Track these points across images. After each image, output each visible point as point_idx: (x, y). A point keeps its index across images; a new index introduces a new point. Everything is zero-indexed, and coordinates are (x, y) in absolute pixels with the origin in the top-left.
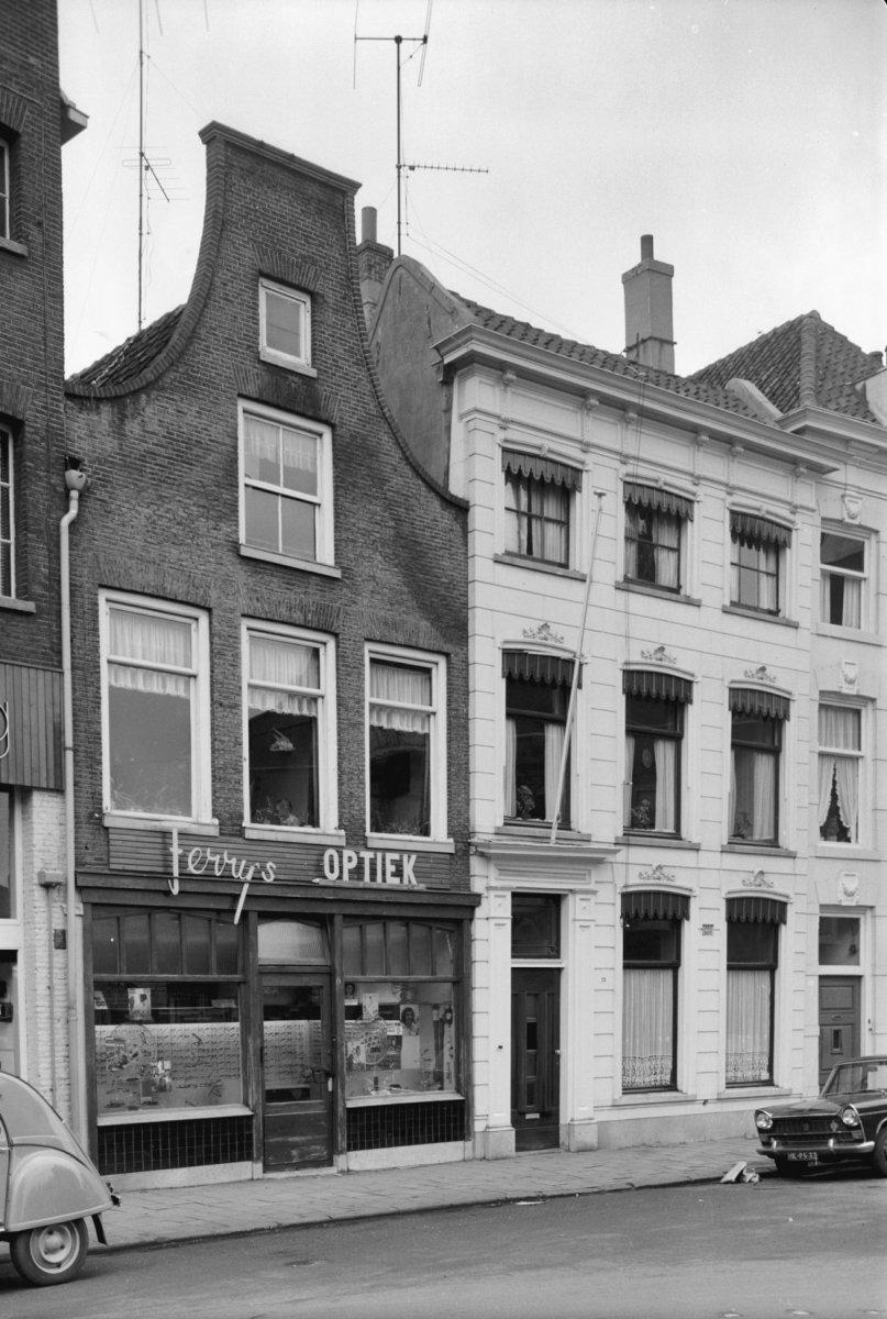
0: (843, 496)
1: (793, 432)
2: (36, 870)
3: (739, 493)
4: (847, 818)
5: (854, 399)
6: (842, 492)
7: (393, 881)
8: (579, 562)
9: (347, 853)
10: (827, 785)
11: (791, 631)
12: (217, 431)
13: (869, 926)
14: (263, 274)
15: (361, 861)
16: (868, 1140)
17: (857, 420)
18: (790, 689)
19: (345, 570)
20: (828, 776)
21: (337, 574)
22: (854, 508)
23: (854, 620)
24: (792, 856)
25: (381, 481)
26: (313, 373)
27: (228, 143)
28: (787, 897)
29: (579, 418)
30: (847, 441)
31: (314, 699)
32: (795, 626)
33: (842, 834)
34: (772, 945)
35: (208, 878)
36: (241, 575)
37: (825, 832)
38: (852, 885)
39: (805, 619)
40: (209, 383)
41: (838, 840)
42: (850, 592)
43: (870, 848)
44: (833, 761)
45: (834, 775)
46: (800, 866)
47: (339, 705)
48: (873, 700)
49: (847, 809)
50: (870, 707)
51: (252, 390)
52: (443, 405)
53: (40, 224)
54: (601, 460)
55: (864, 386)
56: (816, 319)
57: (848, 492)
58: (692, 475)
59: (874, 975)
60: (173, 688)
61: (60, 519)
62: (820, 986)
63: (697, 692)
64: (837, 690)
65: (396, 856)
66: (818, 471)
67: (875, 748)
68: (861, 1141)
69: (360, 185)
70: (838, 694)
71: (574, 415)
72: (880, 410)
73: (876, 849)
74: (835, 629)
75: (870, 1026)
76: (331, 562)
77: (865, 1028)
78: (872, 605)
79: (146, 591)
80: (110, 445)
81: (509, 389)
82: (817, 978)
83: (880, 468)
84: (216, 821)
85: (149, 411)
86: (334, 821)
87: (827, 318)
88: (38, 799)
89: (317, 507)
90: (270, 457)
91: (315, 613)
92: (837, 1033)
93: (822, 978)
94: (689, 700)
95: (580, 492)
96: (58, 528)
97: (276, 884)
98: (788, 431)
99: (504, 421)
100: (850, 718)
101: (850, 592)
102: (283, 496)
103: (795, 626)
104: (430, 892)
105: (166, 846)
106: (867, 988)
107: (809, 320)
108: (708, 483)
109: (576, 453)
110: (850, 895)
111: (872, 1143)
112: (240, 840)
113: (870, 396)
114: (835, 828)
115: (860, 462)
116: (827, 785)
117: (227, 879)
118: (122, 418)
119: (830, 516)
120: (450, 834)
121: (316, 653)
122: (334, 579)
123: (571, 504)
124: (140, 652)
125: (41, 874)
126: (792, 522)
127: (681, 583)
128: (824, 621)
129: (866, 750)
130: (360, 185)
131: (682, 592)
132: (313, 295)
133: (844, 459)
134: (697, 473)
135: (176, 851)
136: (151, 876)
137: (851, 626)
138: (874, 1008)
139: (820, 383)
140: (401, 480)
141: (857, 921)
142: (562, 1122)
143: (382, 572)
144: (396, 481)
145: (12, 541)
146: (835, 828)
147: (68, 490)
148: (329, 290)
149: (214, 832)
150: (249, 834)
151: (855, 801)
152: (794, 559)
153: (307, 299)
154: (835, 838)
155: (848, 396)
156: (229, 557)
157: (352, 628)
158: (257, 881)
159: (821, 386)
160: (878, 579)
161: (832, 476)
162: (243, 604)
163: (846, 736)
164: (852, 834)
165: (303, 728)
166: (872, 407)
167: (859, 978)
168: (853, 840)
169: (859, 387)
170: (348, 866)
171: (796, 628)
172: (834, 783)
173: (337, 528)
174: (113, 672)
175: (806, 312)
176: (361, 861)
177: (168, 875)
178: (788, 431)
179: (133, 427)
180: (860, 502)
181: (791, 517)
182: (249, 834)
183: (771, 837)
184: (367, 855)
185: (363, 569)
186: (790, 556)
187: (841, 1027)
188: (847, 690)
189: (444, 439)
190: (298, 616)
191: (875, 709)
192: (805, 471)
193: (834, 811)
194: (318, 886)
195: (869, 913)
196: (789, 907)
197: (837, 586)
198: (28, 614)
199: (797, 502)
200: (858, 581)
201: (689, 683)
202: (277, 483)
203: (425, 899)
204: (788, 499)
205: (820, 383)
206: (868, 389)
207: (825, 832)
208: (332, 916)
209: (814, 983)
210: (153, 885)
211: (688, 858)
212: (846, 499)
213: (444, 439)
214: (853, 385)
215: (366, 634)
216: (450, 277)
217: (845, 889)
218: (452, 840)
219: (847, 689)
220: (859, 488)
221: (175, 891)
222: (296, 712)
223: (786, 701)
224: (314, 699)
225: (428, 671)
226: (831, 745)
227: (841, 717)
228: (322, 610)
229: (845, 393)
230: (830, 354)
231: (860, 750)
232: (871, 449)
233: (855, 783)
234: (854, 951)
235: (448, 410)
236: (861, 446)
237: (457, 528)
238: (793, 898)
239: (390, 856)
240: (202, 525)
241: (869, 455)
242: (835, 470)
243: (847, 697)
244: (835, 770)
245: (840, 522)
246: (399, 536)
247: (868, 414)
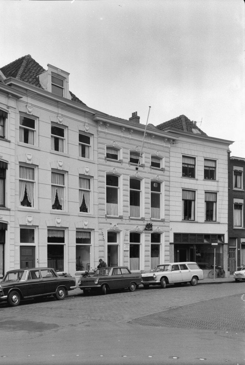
0: (84, 125)
1: (8, 85)
3: (11, 108)
4: (30, 199)
5: (35, 80)
6: (26, 105)
8: (7, 137)
10: (23, 190)
11: (8, 143)
13: (93, 234)
16: (5, 295)
17: (34, 86)
18: (7, 160)
20: (23, 188)
22: (30, 110)
23: (32, 142)
24: (9, 210)
28: (7, 222)
29: (7, 101)
30: (26, 90)
32: (9, 142)
33: (29, 205)
34: (4, 236)
37: (23, 203)
38: (59, 221)
39: (12, 140)
41: (28, 206)
42: (31, 135)
43: (67, 211)
44: (25, 183)
45: (26, 187)
46: (12, 213)
48: (38, 166)
49: (30, 198)
50: (37, 168)
54: (12, 110)
55: (39, 77)
56: (29, 57)
57: (28, 105)
58: (7, 105)
59: (39, 246)
62: (20, 248)
63: (9, 166)
64: (25, 162)
66: (17, 98)
67: (68, 185)
68: (3, 296)
70: (84, 175)
71: (5, 98)
72: (43, 84)
73: (39, 209)
74: (83, 159)
75: (38, 261)
77: (36, 261)
78: (37, 139)
81: (9, 99)
82: (19, 247)
83: (51, 104)
87: (33, 57)
92: (27, 263)
93: (21, 246)
94: (6, 168)
95: (7, 118)
98: (6, 84)
99: (8, 106)
100: (61, 177)
101: (31, 135)
103: (9, 142)
106: (37, 249)
107: (27, 57)
108: (12, 108)
110: (59, 223)
111: (6, 296)
113: (40, 80)
114: (26, 202)
115: (32, 97)
116: (23, 190)
119: (81, 130)
123: (5, 121)
126: (8, 111)
127: (5, 136)
128: (80, 156)
129: (36, 180)
131: (5, 138)
133: (26, 95)
134: (8, 105)
137: (31, 144)
138: (39, 256)
139: (24, 74)
141: (34, 230)
146: (26, 202)
151: (33, 195)
152: (9, 122)
154: (26, 205)
159: (25, 74)
160: (39, 131)
161: (21, 99)
163: (29, 175)
164: (32, 204)
166: (41, 83)
167: (35, 247)
168: (32, 206)
169: (37, 76)
171: (10, 142)
172: (26, 189)
174: (80, 193)
175: (27, 55)
178: (6, 84)
180: (32, 108)
181: (7, 109)
183: (3, 204)
186: (8, 121)
187: (28, 261)
188: (59, 168)
191: (68, 174)
192: (11, 96)
193: (57, 200)
195: (67, 229)
196: (8, 225)
197: (26, 133)
199: (9, 105)
200: (63, 140)
201: (7, 164)
204: (6, 104)
205: (24, 74)
206: (40, 77)
207: (23, 203)
209: (18, 249)
211: (7, 212)
212: (27, 107)
214: (36, 76)
216: (110, 115)
217: (57, 222)
219: (60, 168)
220: (32, 104)
223: (6, 164)
226: (24, 178)
227: (28, 170)
229: (32, 77)
230: (31, 67)
231: (34, 180)
232: (65, 105)
233: (33, 189)
234: (33, 238)
236: (33, 93)
238: (9, 222)
241: (35, 95)
242: (22, 97)
243: (60, 170)
244: (26, 185)
245: (57, 123)
247: (40, 86)
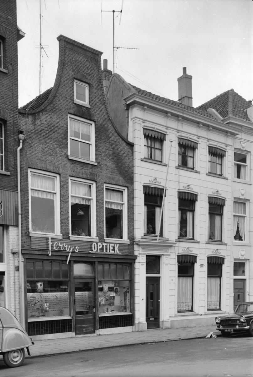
0: (240, 142)
1: (226, 123)
2: (10, 249)
3: (211, 141)
4: (242, 234)
5: (244, 114)
6: (240, 141)
7: (112, 252)
9: (99, 244)
10: (236, 224)
11: (226, 180)
12: (62, 123)
13: (248, 265)
14: (75, 78)
15: (103, 246)
16: (248, 326)
17: (244, 120)
18: (225, 197)
19: (98, 163)
20: (236, 222)
21: (96, 164)
22: (244, 145)
23: (244, 177)
24: (226, 245)
25: (109, 138)
26: (89, 107)
27: (65, 41)
28: (225, 256)
29: (165, 120)
30: (242, 126)
31: (89, 200)
32: (227, 179)
33: (240, 238)
34: (220, 270)
35: (59, 251)
36: (69, 164)
37: (235, 238)
38: (243, 253)
39: (230, 177)
40: (60, 109)
41: (239, 240)
42: (242, 169)
43: (248, 242)
44: (238, 218)
45: (238, 222)
46: (228, 247)
47: (97, 201)
48: (249, 200)
50: (248, 202)
51: (72, 111)
52: (126, 116)
53: (11, 64)
54: (171, 131)
55: (247, 110)
56: (233, 91)
57: (242, 141)
58: (197, 136)
59: (249, 279)
60: (49, 197)
61: (17, 148)
62: (234, 282)
63: (199, 198)
64: (239, 197)
65: (113, 245)
66: (233, 135)
67: (250, 214)
68: (246, 326)
69: (103, 53)
70: (239, 198)
71: (164, 118)
72: (251, 117)
73: (250, 243)
74: (238, 180)
75: (248, 293)
76: (94, 161)
77: (247, 294)
78: (249, 173)
80: (31, 127)
81: (145, 111)
82: (233, 280)
83: (251, 134)
84: (62, 235)
85: (42, 117)
86: (95, 235)
87: (236, 91)
88: (11, 228)
89: (90, 145)
90: (77, 130)
91: (90, 175)
92: (239, 295)
93: (234, 279)
94: (196, 200)
95: (166, 141)
96: (17, 151)
97: (79, 253)
98: (225, 123)
99: (144, 120)
100: (243, 205)
101: (242, 169)
102: (81, 142)
103: (227, 179)
104: (123, 255)
105: (47, 242)
106: (247, 282)
107: (231, 92)
108: (202, 138)
110: (242, 256)
111: (249, 327)
112: (68, 240)
113: (248, 113)
114: (238, 237)
115: (245, 132)
116: (236, 224)
117: (65, 251)
118: (35, 119)
119: (237, 147)
120: (128, 238)
121: (90, 187)
122: (95, 166)
123: (163, 144)
124: (40, 186)
125: (12, 250)
126: (226, 149)
127: (194, 167)
128: (235, 178)
129: (247, 214)
130: (103, 53)
131: (195, 169)
132: (89, 84)
133: (241, 131)
134: (199, 135)
135: (50, 243)
136: (43, 250)
137: (243, 179)
138: (249, 288)
139: (234, 109)
140: (114, 137)
141: (244, 263)
142: (160, 321)
143: (109, 163)
144: (113, 138)
145: (3, 155)
146: (238, 237)
147: (19, 140)
148: (94, 83)
149: (61, 238)
150: (71, 238)
151: (244, 229)
152: (227, 160)
153: (88, 85)
154: (238, 239)
156: (65, 159)
157: (100, 180)
158: (73, 252)
160: (250, 165)
161: (237, 136)
162: (69, 173)
163: (241, 210)
164: (243, 238)
165: (87, 208)
166: (249, 116)
167: (245, 280)
168: (243, 240)
169: (245, 110)
170: (99, 248)
171: (227, 179)
172: (238, 224)
173: (96, 151)
174: (32, 192)
175: (230, 89)
176: (103, 246)
177: (48, 250)
178: (225, 123)
179: (38, 122)
180: (245, 143)
181: (226, 148)
182: (71, 238)
183: (220, 239)
184: (105, 244)
185: (104, 163)
186: (225, 159)
187: (240, 294)
188: (242, 197)
189: (127, 125)
190: (85, 176)
191: (250, 203)
192: (230, 135)
193: (238, 232)
194: (91, 253)
195: (248, 261)
196: (225, 259)
197: (239, 168)
198: (8, 176)
199: (227, 143)
200: (245, 166)
201: (197, 195)
202: (79, 138)
203: (121, 257)
204: (225, 143)
205: (234, 109)
206: (248, 111)
207: (235, 238)
208: (95, 262)
209: (232, 281)
210: (44, 253)
211: (196, 245)
212: (241, 143)
213: (127, 125)
214: (243, 110)
215: (104, 181)
216: (128, 79)
217: (241, 254)
218: (129, 240)
219: (242, 197)
220: (245, 139)
221: (50, 255)
222: (84, 203)
223: (224, 200)
224: (89, 200)
225: (122, 192)
226: (237, 213)
227: (240, 205)
228: (92, 174)
229: (241, 112)
230: (237, 101)
231: (245, 214)
232: (248, 128)
233: (244, 224)
234: (244, 272)
235: (128, 117)
236: (246, 128)
237: (130, 151)
238: (226, 257)
239: (111, 245)
240: (58, 150)
241: (248, 130)
242: (238, 134)
243: (242, 199)
244: (238, 220)
245: (240, 149)
246: (114, 153)
247: (248, 118)
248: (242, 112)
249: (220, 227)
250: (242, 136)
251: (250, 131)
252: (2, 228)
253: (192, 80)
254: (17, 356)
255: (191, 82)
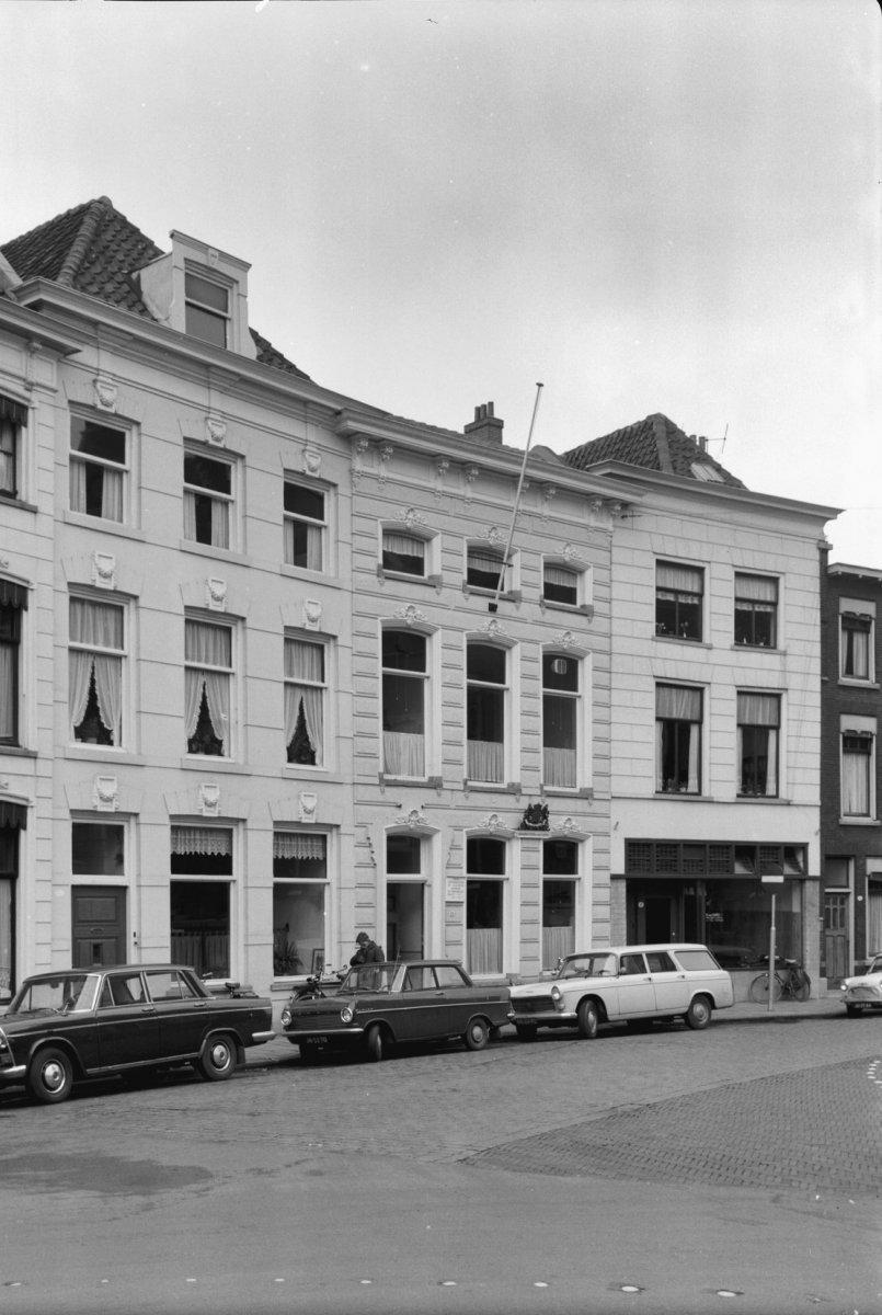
0: (304, 451)
1: (29, 306)
3: (39, 389)
4: (108, 718)
5: (126, 287)
6: (94, 377)
10: (83, 684)
11: (28, 516)
13: (335, 842)
17: (122, 309)
18: (26, 576)
20: (84, 677)
22: (108, 396)
23: (116, 513)
24: (32, 756)
28: (27, 800)
29: (24, 363)
30: (95, 324)
32: (34, 511)
33: (104, 737)
34: (13, 849)
37: (82, 733)
38: (212, 796)
39: (45, 505)
41: (99, 742)
42: (110, 487)
43: (241, 761)
44: (91, 659)
45: (93, 674)
46: (43, 767)
48: (136, 598)
49: (108, 712)
50: (132, 604)
54: (43, 397)
55: (139, 276)
56: (106, 205)
57: (100, 378)
58: (24, 380)
59: (139, 886)
62: (73, 895)
63: (32, 599)
64: (90, 583)
66: (61, 353)
67: (245, 666)
70: (302, 630)
71: (18, 354)
72: (153, 301)
73: (140, 754)
74: (299, 571)
75: (135, 940)
77: (131, 940)
78: (134, 501)
79: (629, 694)
81: (34, 355)
82: (69, 890)
83: (183, 373)
87: (119, 206)
92: (97, 947)
93: (74, 887)
94: (23, 606)
95: (26, 426)
98: (22, 304)
99: (28, 383)
100: (221, 636)
101: (110, 487)
103: (34, 511)
106: (132, 897)
107: (98, 205)
108: (42, 390)
109: (21, 390)
110: (211, 805)
113: (144, 287)
114: (93, 728)
115: (115, 349)
116: (83, 684)
119: (293, 468)
123: (18, 437)
126: (28, 400)
127: (18, 488)
128: (286, 562)
129: (129, 648)
131: (18, 498)
133: (93, 341)
134: (30, 379)
137: (113, 519)
138: (140, 923)
139: (87, 265)
141: (121, 828)
146: (93, 728)
151: (118, 702)
152: (31, 441)
154: (95, 740)
155: (119, 283)
159: (88, 268)
160: (140, 471)
161: (75, 357)
163: (106, 631)
164: (115, 737)
166: (146, 299)
167: (124, 888)
168: (115, 744)
169: (134, 275)
171: (35, 512)
172: (93, 682)
175: (97, 197)
178: (22, 304)
180: (115, 389)
181: (27, 394)
183: (10, 735)
186: (27, 436)
187: (99, 941)
188: (214, 606)
191: (244, 628)
192: (40, 347)
193: (204, 721)
195: (241, 826)
196: (29, 811)
197: (95, 478)
199: (33, 378)
200: (226, 503)
201: (24, 589)
204: (22, 374)
205: (87, 265)
206: (142, 277)
207: (82, 733)
209: (65, 896)
211: (24, 765)
212: (99, 385)
214: (130, 272)
216: (395, 414)
217: (205, 799)
219: (215, 606)
220: (114, 375)
223: (22, 591)
226: (88, 642)
227: (100, 613)
229: (116, 278)
230: (112, 241)
231: (123, 648)
232: (234, 378)
233: (118, 682)
234: (120, 859)
236: (118, 334)
238: (34, 801)
241: (125, 343)
242: (78, 351)
243: (215, 613)
244: (93, 668)
245: (205, 444)
247: (144, 310)
248: (119, 278)
249: (10, 697)
250: (87, 355)
251: (134, 346)
252: (67, 710)
253: (503, 430)
254: (304, 947)
255: (501, 433)
